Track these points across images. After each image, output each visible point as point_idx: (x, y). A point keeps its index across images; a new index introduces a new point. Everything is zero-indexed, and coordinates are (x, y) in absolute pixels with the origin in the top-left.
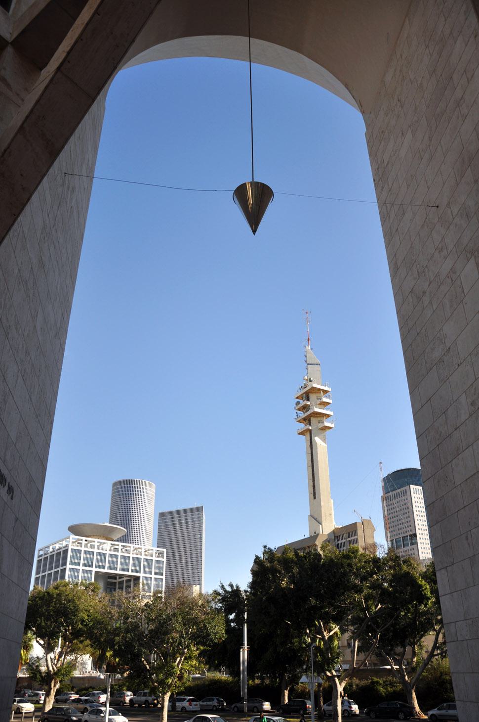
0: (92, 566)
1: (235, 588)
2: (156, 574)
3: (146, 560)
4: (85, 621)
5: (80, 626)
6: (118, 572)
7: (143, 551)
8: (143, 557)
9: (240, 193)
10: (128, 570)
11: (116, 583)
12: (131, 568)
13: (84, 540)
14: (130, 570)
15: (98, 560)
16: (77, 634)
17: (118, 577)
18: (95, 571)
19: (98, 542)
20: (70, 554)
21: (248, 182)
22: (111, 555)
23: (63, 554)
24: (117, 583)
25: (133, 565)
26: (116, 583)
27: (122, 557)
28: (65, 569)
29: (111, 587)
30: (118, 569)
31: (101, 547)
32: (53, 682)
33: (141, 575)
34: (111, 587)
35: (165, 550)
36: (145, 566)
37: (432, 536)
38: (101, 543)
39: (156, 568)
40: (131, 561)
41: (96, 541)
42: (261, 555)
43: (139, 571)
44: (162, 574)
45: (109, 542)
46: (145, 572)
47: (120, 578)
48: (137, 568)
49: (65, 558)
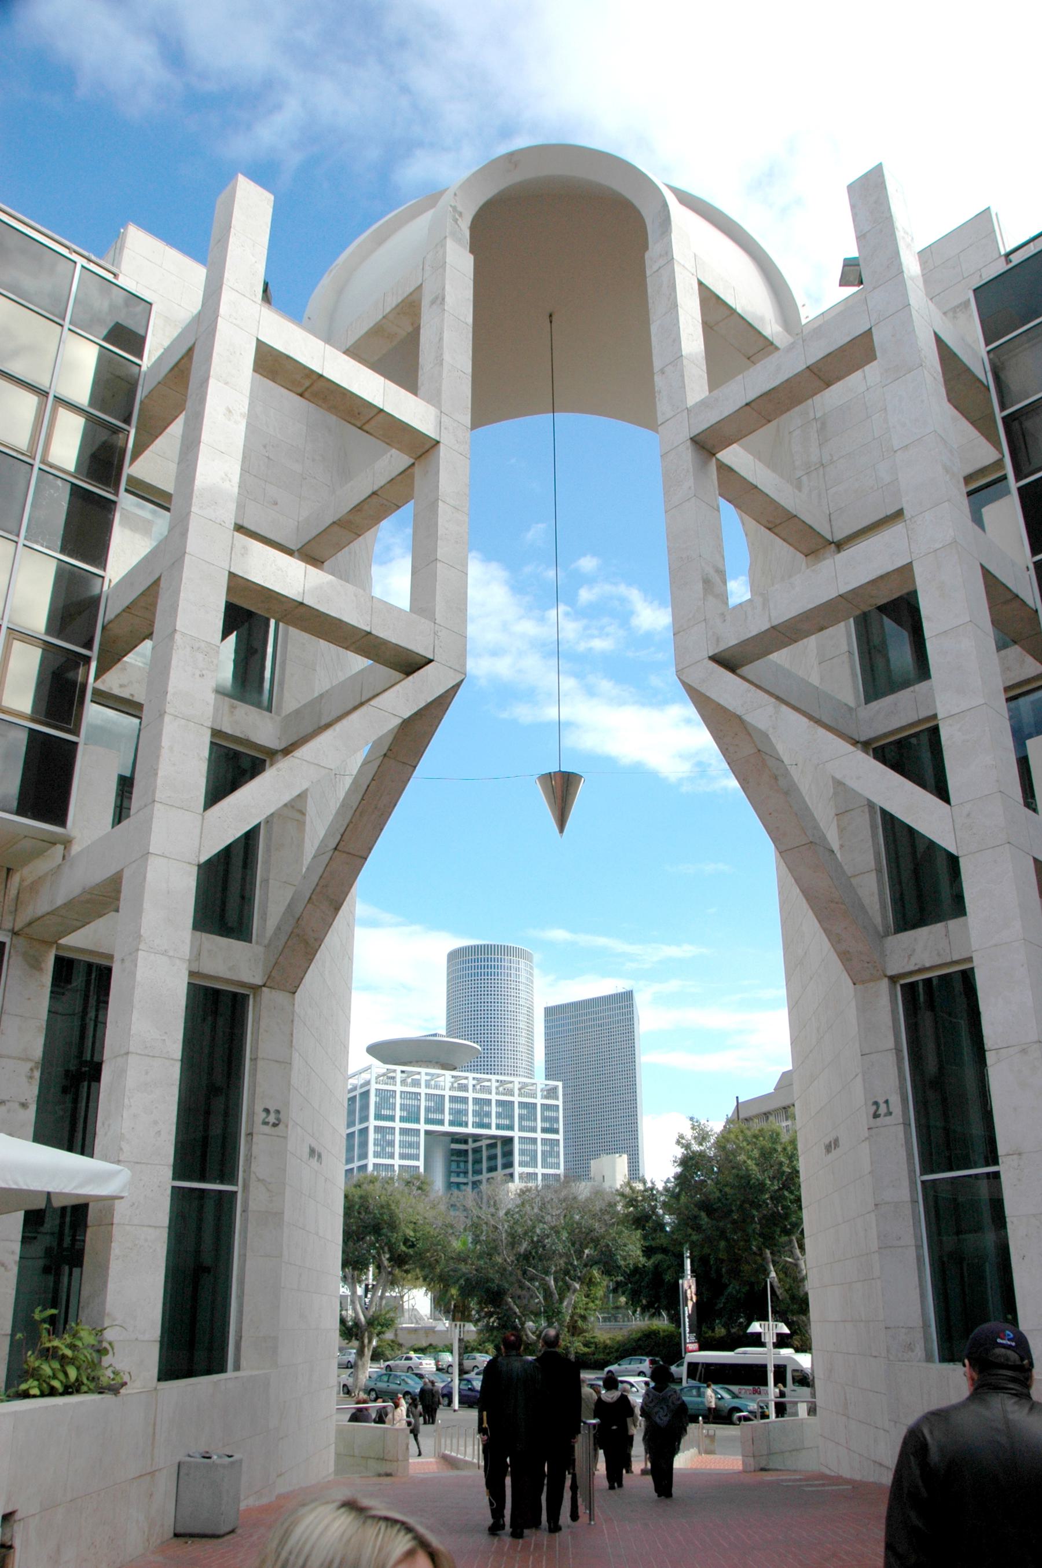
0: (418, 1121)
1: (649, 1185)
2: (544, 1130)
3: (522, 1105)
4: (409, 1240)
5: (403, 1248)
6: (470, 1130)
7: (517, 1086)
8: (516, 1099)
9: (547, 779)
10: (488, 1126)
12: (494, 1121)
13: (399, 1072)
14: (494, 1126)
15: (428, 1110)
16: (399, 1260)
17: (470, 1140)
18: (400, 1128)
19: (427, 1074)
20: (373, 1099)
22: (453, 1099)
23: (361, 1100)
24: (470, 1153)
25: (499, 1115)
27: (476, 1101)
28: (367, 1128)
29: (458, 1159)
31: (433, 1083)
32: (366, 1334)
33: (516, 1134)
34: (458, 1159)
35: (560, 1084)
36: (521, 1117)
38: (432, 1075)
39: (544, 1119)
40: (494, 1109)
41: (423, 1073)
42: (689, 1134)
44: (556, 1131)
45: (448, 1073)
46: (522, 1129)
47: (475, 1141)
48: (507, 1122)
49: (365, 1107)
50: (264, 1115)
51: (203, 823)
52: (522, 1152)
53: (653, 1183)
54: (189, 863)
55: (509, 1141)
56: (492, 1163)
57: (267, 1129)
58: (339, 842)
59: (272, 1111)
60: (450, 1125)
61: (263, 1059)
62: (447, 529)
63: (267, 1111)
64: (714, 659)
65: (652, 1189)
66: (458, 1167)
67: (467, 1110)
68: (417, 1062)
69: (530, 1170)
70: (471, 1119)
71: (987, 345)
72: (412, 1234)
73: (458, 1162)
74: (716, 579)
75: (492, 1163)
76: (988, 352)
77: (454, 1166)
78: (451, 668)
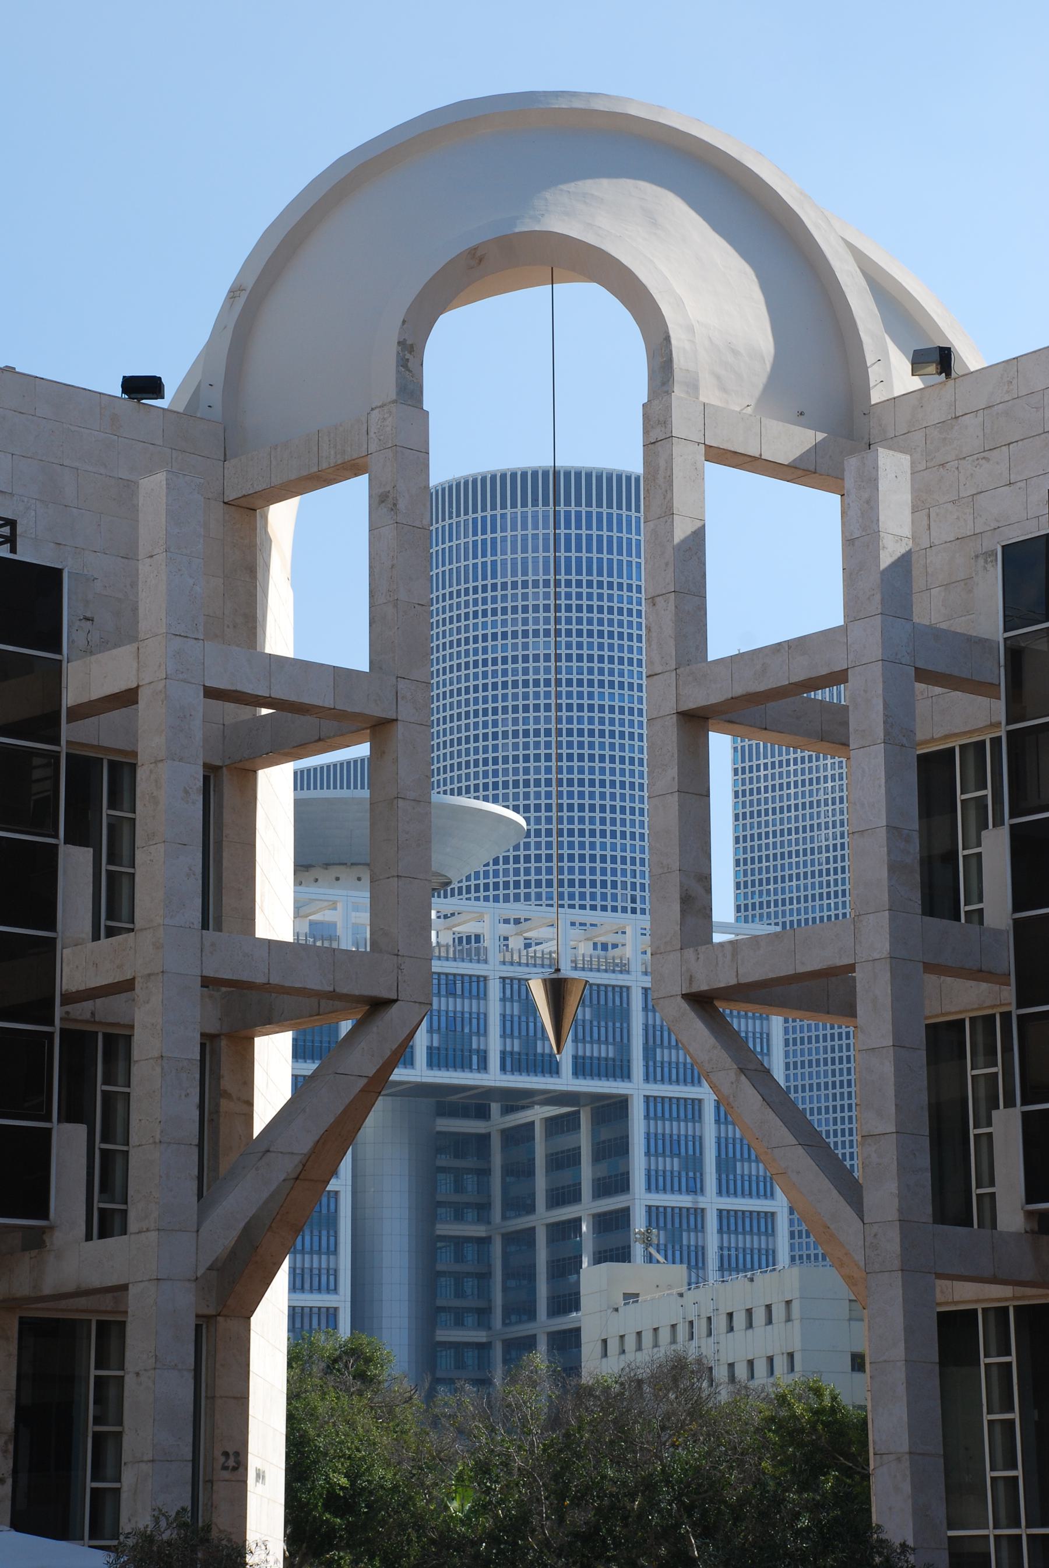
1: (827, 1402)
6: (494, 1077)
17: (495, 1108)
21: (973, 1020)
37: (274, 1264)
43: (620, 1069)
47: (508, 1110)
50: (222, 1459)
51: (197, 1239)
52: (655, 1146)
53: (834, 1398)
54: (189, 1280)
55: (619, 1106)
56: (565, 1177)
57: (226, 1475)
58: (301, 1172)
59: (231, 1454)
60: (430, 1065)
61: (221, 1397)
62: (407, 833)
63: (226, 1454)
64: (688, 997)
65: (833, 1410)
66: (459, 1188)
67: (482, 1018)
68: (327, 866)
69: (683, 1201)
70: (494, 1045)
71: (1005, 631)
72: (344, 1481)
75: (565, 1177)
76: (1005, 639)
77: (445, 1191)
78: (415, 1002)
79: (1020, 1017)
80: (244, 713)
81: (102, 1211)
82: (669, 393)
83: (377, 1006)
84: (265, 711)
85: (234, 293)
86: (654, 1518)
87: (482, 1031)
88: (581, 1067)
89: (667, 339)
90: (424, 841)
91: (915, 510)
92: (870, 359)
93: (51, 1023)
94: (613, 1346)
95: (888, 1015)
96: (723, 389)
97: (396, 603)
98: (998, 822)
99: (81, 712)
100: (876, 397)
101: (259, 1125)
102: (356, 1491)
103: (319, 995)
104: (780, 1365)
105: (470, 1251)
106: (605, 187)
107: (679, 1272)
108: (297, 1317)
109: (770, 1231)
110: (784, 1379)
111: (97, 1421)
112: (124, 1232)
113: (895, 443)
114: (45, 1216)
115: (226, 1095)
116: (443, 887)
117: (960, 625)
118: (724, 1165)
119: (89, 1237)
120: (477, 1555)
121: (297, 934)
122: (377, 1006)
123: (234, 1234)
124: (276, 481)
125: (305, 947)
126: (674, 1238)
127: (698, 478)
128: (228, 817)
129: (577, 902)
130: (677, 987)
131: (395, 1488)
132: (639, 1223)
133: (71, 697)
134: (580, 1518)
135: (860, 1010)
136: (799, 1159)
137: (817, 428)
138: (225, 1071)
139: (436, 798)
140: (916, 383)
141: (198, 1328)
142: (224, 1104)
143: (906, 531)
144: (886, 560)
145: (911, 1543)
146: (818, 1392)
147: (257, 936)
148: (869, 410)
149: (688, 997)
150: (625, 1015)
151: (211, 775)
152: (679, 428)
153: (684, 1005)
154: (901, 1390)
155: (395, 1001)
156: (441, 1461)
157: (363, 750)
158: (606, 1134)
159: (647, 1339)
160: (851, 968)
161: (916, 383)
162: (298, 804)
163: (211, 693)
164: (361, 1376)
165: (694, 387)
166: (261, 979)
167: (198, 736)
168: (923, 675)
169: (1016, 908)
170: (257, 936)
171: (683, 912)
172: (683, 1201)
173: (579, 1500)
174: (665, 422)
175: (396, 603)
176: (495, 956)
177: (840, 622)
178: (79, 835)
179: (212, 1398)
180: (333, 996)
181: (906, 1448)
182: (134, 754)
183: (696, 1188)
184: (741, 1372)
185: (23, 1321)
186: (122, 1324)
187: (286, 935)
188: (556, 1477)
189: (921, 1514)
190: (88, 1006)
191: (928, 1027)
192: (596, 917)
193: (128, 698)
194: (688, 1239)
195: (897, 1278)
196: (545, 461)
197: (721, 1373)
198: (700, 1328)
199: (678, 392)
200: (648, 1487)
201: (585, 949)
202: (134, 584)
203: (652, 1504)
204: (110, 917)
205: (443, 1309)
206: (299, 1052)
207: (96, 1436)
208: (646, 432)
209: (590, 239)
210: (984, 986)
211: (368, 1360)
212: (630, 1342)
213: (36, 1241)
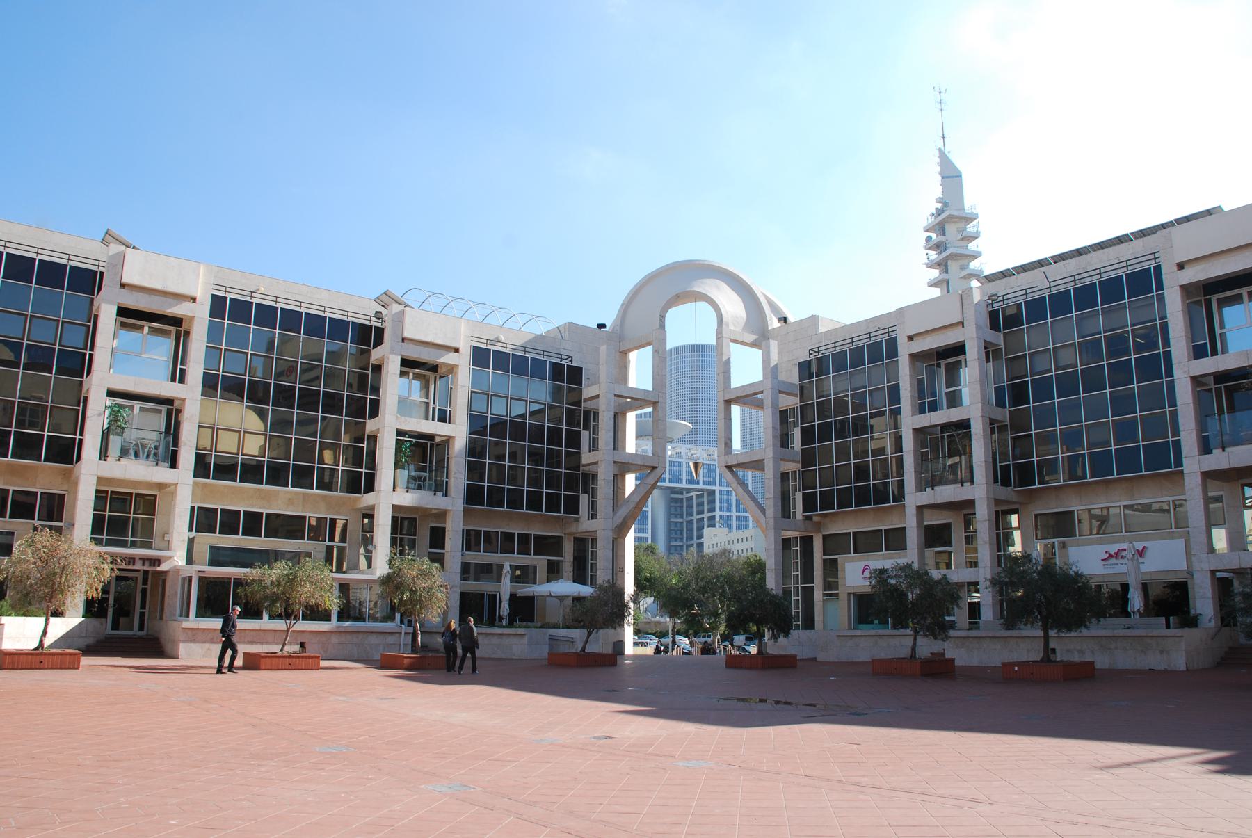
6: (684, 485)
11: (682, 499)
14: (701, 482)
17: (684, 492)
24: (684, 500)
26: (682, 499)
30: (684, 481)
33: (717, 488)
43: (713, 483)
47: (687, 493)
55: (712, 493)
56: (701, 508)
64: (726, 466)
69: (728, 514)
73: (676, 507)
74: (729, 442)
75: (701, 508)
77: (673, 510)
79: (802, 471)
80: (624, 400)
81: (592, 514)
82: (722, 327)
83: (654, 468)
84: (629, 400)
85: (622, 305)
86: (718, 584)
87: (682, 475)
88: (704, 483)
89: (722, 315)
90: (665, 430)
91: (778, 354)
92: (768, 320)
93: (579, 471)
94: (711, 546)
95: (772, 470)
96: (734, 326)
97: (659, 375)
98: (798, 426)
99: (587, 400)
100: (770, 328)
101: (626, 496)
102: (651, 578)
103: (640, 465)
104: (749, 550)
105: (678, 525)
106: (707, 281)
107: (727, 529)
108: (636, 539)
109: (748, 521)
110: (749, 553)
111: (591, 560)
112: (596, 518)
113: (774, 338)
114: (579, 515)
115: (620, 488)
116: (672, 441)
117: (789, 381)
118: (737, 505)
119: (589, 519)
120: (678, 592)
121: (636, 451)
122: (654, 468)
123: (621, 519)
124: (631, 347)
125: (27, 363)
126: (726, 522)
127: (729, 346)
128: (620, 424)
129: (709, 445)
130: (724, 464)
131: (660, 577)
132: (717, 519)
133: (584, 397)
134: (702, 584)
135: (766, 469)
136: (751, 504)
137: (755, 334)
138: (619, 484)
139: (667, 420)
140: (779, 325)
141: (613, 540)
142: (619, 490)
143: (777, 359)
144: (772, 365)
145: (774, 588)
146: (756, 556)
147: (627, 451)
148: (768, 331)
149: (726, 466)
150: (715, 471)
151: (616, 415)
152: (724, 335)
153: (725, 468)
154: (773, 556)
155: (657, 467)
156: (670, 571)
157: (650, 409)
158: (710, 498)
159: (719, 545)
160: (764, 460)
161: (779, 325)
162: (637, 422)
163: (615, 396)
164: (652, 552)
165: (727, 325)
166: (627, 462)
167: (613, 407)
168: (780, 392)
169: (802, 446)
170: (627, 451)
171: (725, 447)
172: (728, 514)
173: (701, 580)
174: (721, 333)
175: (659, 375)
176: (684, 457)
177: (762, 379)
178: (586, 428)
179: (617, 556)
180: (643, 465)
181: (774, 568)
182: (598, 410)
183: (731, 511)
184: (740, 552)
185: (574, 538)
186: (596, 539)
187: (633, 451)
188: (696, 575)
189: (777, 582)
190: (588, 467)
191: (781, 473)
192: (706, 448)
193: (597, 397)
194: (729, 522)
195: (773, 531)
196: (693, 342)
197: (736, 552)
198: (731, 542)
199: (724, 326)
200: (718, 577)
201: (705, 456)
202: (599, 371)
203: (718, 580)
204: (593, 447)
205: (672, 538)
206: (637, 479)
207: (591, 551)
208: (717, 336)
209: (704, 292)
210: (794, 464)
211: (654, 549)
212: (715, 546)
213: (577, 520)
